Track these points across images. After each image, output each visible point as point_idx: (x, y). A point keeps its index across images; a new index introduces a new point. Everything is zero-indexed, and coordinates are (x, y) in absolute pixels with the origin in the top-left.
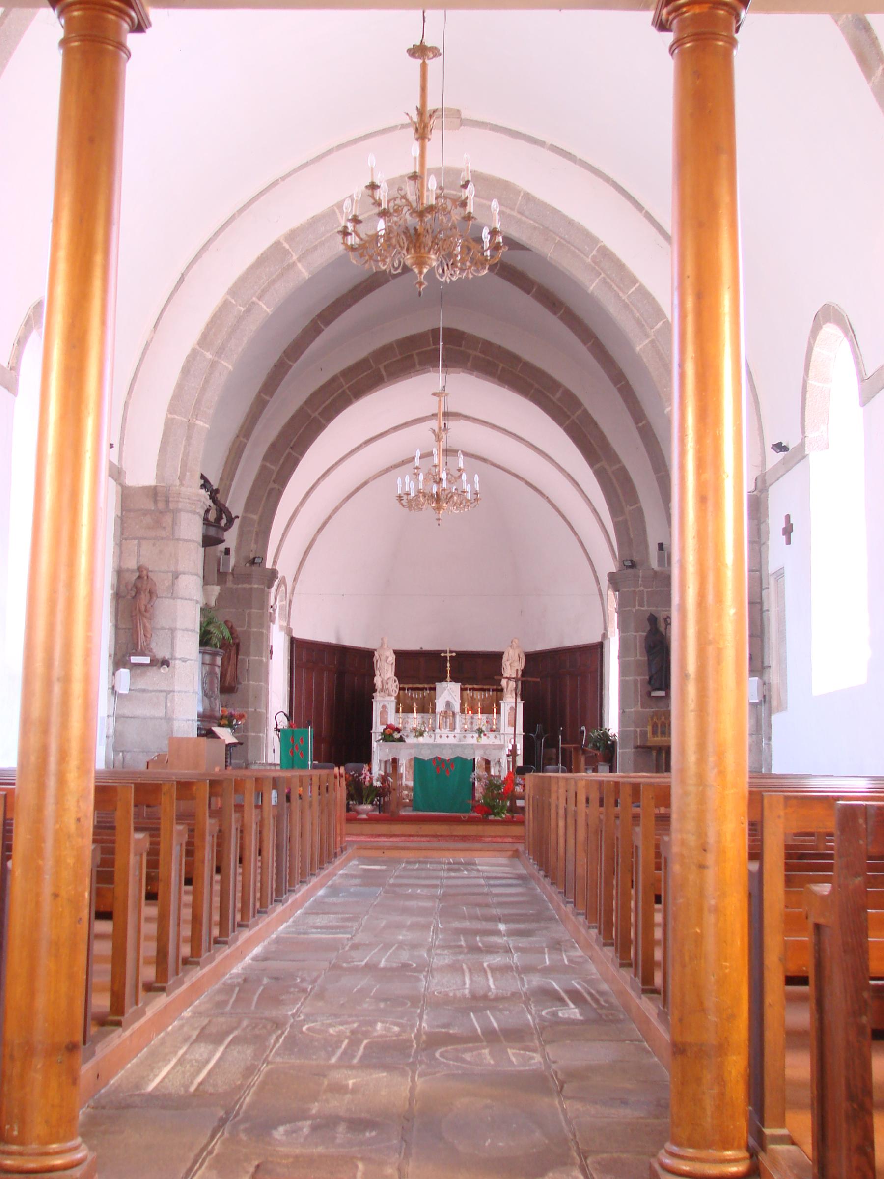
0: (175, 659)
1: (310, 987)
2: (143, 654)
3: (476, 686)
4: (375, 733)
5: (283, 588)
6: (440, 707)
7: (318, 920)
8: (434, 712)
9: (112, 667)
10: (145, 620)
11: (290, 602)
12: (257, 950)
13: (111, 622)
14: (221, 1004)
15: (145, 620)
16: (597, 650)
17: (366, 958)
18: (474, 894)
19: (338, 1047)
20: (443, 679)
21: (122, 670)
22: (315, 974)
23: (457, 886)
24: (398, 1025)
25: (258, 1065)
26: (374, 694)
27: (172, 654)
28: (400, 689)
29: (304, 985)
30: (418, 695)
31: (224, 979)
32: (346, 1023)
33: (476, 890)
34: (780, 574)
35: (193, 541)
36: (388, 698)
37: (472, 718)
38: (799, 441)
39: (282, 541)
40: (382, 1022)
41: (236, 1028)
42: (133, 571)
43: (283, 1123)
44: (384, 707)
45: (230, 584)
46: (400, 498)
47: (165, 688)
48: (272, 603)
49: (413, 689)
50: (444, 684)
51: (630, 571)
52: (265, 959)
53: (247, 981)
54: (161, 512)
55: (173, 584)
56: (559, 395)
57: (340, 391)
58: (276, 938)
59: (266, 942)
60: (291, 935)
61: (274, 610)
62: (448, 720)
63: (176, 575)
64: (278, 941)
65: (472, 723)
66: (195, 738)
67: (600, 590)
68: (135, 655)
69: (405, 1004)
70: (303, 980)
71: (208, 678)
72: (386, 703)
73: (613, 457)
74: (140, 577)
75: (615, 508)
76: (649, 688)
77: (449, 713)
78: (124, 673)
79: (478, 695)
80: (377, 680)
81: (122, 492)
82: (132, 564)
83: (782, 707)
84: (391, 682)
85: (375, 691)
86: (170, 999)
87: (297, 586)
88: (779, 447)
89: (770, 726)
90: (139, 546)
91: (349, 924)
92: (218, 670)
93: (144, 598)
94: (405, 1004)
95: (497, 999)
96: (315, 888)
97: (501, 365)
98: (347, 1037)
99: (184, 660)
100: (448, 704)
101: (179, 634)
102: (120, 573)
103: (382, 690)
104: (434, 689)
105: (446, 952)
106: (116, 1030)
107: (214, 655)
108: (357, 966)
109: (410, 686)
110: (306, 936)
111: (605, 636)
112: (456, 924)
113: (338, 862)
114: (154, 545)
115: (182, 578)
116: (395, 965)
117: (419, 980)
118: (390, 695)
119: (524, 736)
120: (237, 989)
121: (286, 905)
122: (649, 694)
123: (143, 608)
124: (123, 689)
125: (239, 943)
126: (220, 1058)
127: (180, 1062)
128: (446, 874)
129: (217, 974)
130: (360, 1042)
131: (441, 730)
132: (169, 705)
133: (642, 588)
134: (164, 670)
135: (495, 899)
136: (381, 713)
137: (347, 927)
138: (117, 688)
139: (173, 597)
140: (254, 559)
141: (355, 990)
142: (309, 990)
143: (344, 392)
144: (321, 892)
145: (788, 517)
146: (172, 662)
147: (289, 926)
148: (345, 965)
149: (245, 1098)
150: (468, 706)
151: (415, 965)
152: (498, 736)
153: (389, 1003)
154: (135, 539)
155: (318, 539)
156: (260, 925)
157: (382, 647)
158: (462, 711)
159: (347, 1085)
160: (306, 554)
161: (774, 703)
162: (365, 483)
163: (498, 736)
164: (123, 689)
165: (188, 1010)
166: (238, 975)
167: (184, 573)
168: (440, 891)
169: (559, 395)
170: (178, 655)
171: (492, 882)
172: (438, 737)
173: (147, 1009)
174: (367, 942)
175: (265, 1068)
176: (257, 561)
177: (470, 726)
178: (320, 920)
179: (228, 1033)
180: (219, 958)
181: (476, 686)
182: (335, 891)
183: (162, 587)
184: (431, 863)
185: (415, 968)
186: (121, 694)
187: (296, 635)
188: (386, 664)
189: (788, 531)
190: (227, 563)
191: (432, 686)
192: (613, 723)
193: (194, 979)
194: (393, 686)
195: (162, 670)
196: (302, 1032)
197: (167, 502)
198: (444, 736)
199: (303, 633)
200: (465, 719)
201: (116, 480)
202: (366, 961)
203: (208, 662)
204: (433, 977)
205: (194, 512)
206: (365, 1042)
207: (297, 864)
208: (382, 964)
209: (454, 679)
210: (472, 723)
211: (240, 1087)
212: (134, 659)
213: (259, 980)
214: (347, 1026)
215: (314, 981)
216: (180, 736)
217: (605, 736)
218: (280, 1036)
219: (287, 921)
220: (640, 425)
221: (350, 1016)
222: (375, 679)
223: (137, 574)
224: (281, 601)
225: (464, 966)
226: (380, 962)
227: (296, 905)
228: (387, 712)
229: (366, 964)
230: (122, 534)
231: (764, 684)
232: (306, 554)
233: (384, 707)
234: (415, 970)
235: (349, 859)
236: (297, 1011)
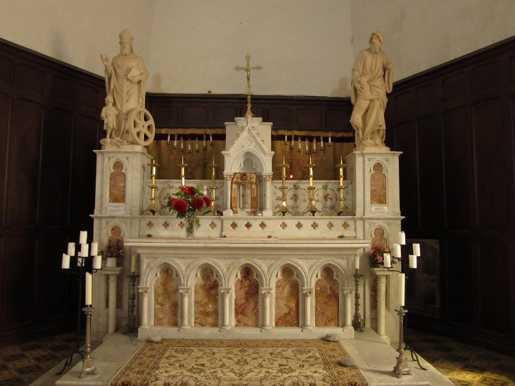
4: (100, 218)
8: (219, 176)
26: (102, 141)
36: (127, 148)
37: (296, 187)
44: (118, 165)
49: (186, 137)
62: (248, 192)
65: (295, 197)
72: (122, 158)
85: (104, 134)
104: (222, 137)
109: (181, 131)
119: (403, 221)
131: (235, 212)
136: (113, 177)
152: (351, 223)
158: (277, 175)
163: (351, 223)
172: (227, 225)
177: (291, 203)
188: (126, 83)
191: (219, 132)
198: (242, 224)
200: (282, 189)
203: (328, 207)
210: (295, 197)
222: (104, 109)
228: (124, 175)
233: (118, 165)
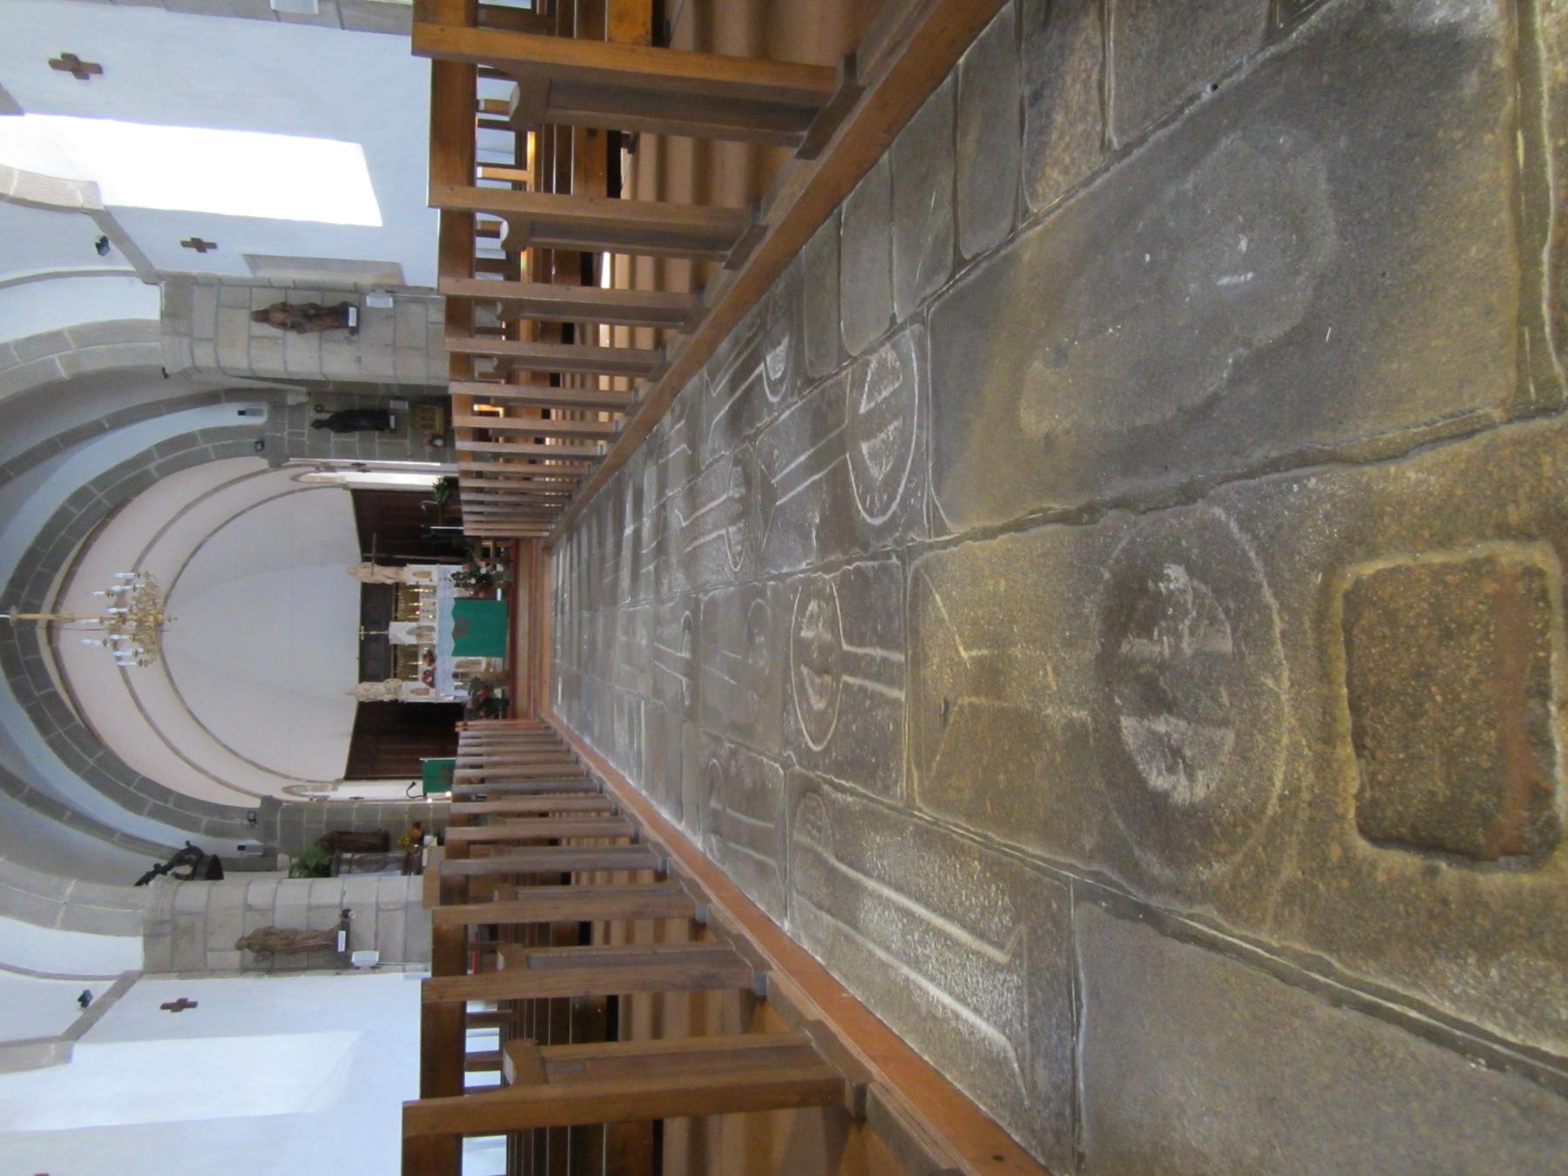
0: (341, 903)
1: (728, 745)
2: (335, 940)
3: (393, 608)
5: (295, 790)
6: (412, 640)
7: (622, 741)
8: (416, 646)
9: (350, 971)
10: (298, 938)
11: (309, 781)
12: (666, 814)
13: (299, 975)
14: (762, 868)
15: (298, 938)
16: (364, 499)
17: (676, 677)
18: (589, 578)
19: (862, 689)
20: (386, 638)
21: (353, 959)
22: (704, 739)
23: (580, 599)
24: (803, 606)
25: (916, 825)
27: (336, 907)
28: (395, 676)
29: (724, 753)
30: (401, 661)
31: (715, 862)
32: (801, 685)
33: (584, 578)
34: (253, 260)
35: (209, 891)
38: (89, 220)
39: (238, 790)
40: (800, 629)
41: (820, 861)
42: (243, 955)
43: (1140, 781)
44: (412, 692)
45: (276, 844)
46: (141, 663)
47: (374, 912)
48: (307, 799)
50: (391, 637)
51: (267, 445)
52: (680, 804)
53: (717, 827)
54: (175, 929)
55: (258, 910)
56: (73, 510)
57: (66, 738)
58: (647, 790)
59: (654, 803)
60: (643, 774)
61: (315, 797)
63: (249, 907)
64: (652, 788)
65: (428, 611)
66: (425, 880)
67: (302, 490)
68: (336, 946)
69: (760, 608)
70: (715, 755)
71: (365, 867)
73: (144, 457)
74: (249, 947)
75: (201, 459)
76: (387, 431)
77: (419, 632)
78: (356, 957)
79: (402, 606)
80: (387, 698)
81: (149, 973)
82: (235, 957)
83: (396, 269)
84: (388, 686)
86: (774, 963)
87: (294, 775)
88: (102, 245)
89: (418, 288)
90: (213, 950)
91: (626, 705)
92: (357, 856)
93: (272, 941)
94: (760, 608)
95: (747, 480)
96: (583, 746)
97: (39, 568)
98: (837, 679)
99: (343, 893)
100: (410, 632)
101: (315, 901)
102: (244, 970)
103: (396, 694)
104: (395, 646)
105: (665, 581)
106: (874, 1097)
107: (340, 861)
108: (688, 686)
110: (644, 755)
111: (345, 486)
112: (625, 583)
113: (554, 725)
114: (212, 933)
115: (251, 900)
116: (687, 638)
117: (712, 601)
118: (401, 686)
120: (732, 845)
121: (604, 779)
122: (393, 431)
123: (284, 942)
124: (375, 956)
125: (661, 840)
126: (899, 889)
127: (917, 964)
128: (567, 616)
129: (708, 870)
130: (846, 656)
132: (392, 907)
133: (285, 433)
134: (353, 915)
135: (595, 551)
137: (630, 709)
138: (373, 964)
139: (273, 910)
140: (250, 820)
141: (732, 682)
142: (733, 746)
143: (66, 733)
144: (587, 740)
145: (185, 244)
146: (345, 907)
147: (631, 774)
148: (687, 703)
149: (1034, 856)
150: (411, 615)
151: (687, 613)
153: (756, 631)
154: (205, 956)
155: (248, 756)
156: (634, 811)
157: (355, 695)
158: (416, 620)
159: (978, 661)
160: (260, 767)
161: (395, 282)
162: (190, 713)
164: (375, 956)
165: (778, 923)
166: (706, 842)
167: (246, 898)
168: (586, 614)
169: (73, 510)
170: (337, 900)
171: (575, 565)
173: (811, 1018)
174: (651, 680)
175: (926, 813)
176: (252, 816)
178: (622, 739)
179: (832, 872)
180: (687, 871)
181: (393, 608)
182: (585, 726)
183: (261, 923)
184: (555, 633)
185: (692, 612)
186: (380, 958)
187: (342, 773)
189: (200, 245)
190: (254, 848)
192: (428, 481)
193: (729, 914)
194: (392, 683)
195: (354, 917)
196: (827, 750)
197: (162, 922)
199: (340, 767)
201: (134, 982)
202: (680, 677)
204: (707, 583)
205: (175, 892)
206: (845, 647)
207: (557, 769)
208: (686, 655)
209: (387, 627)
211: (988, 864)
212: (341, 947)
213: (715, 814)
214: (808, 685)
215: (717, 740)
216: (421, 893)
217: (438, 487)
218: (831, 783)
219: (623, 778)
220: (107, 426)
221: (787, 680)
223: (247, 950)
224: (307, 790)
225: (689, 549)
226: (682, 658)
227: (603, 765)
229: (686, 675)
230: (200, 970)
231: (373, 291)
232: (260, 767)
233: (412, 692)
234: (695, 612)
235: (552, 715)
236: (775, 760)
